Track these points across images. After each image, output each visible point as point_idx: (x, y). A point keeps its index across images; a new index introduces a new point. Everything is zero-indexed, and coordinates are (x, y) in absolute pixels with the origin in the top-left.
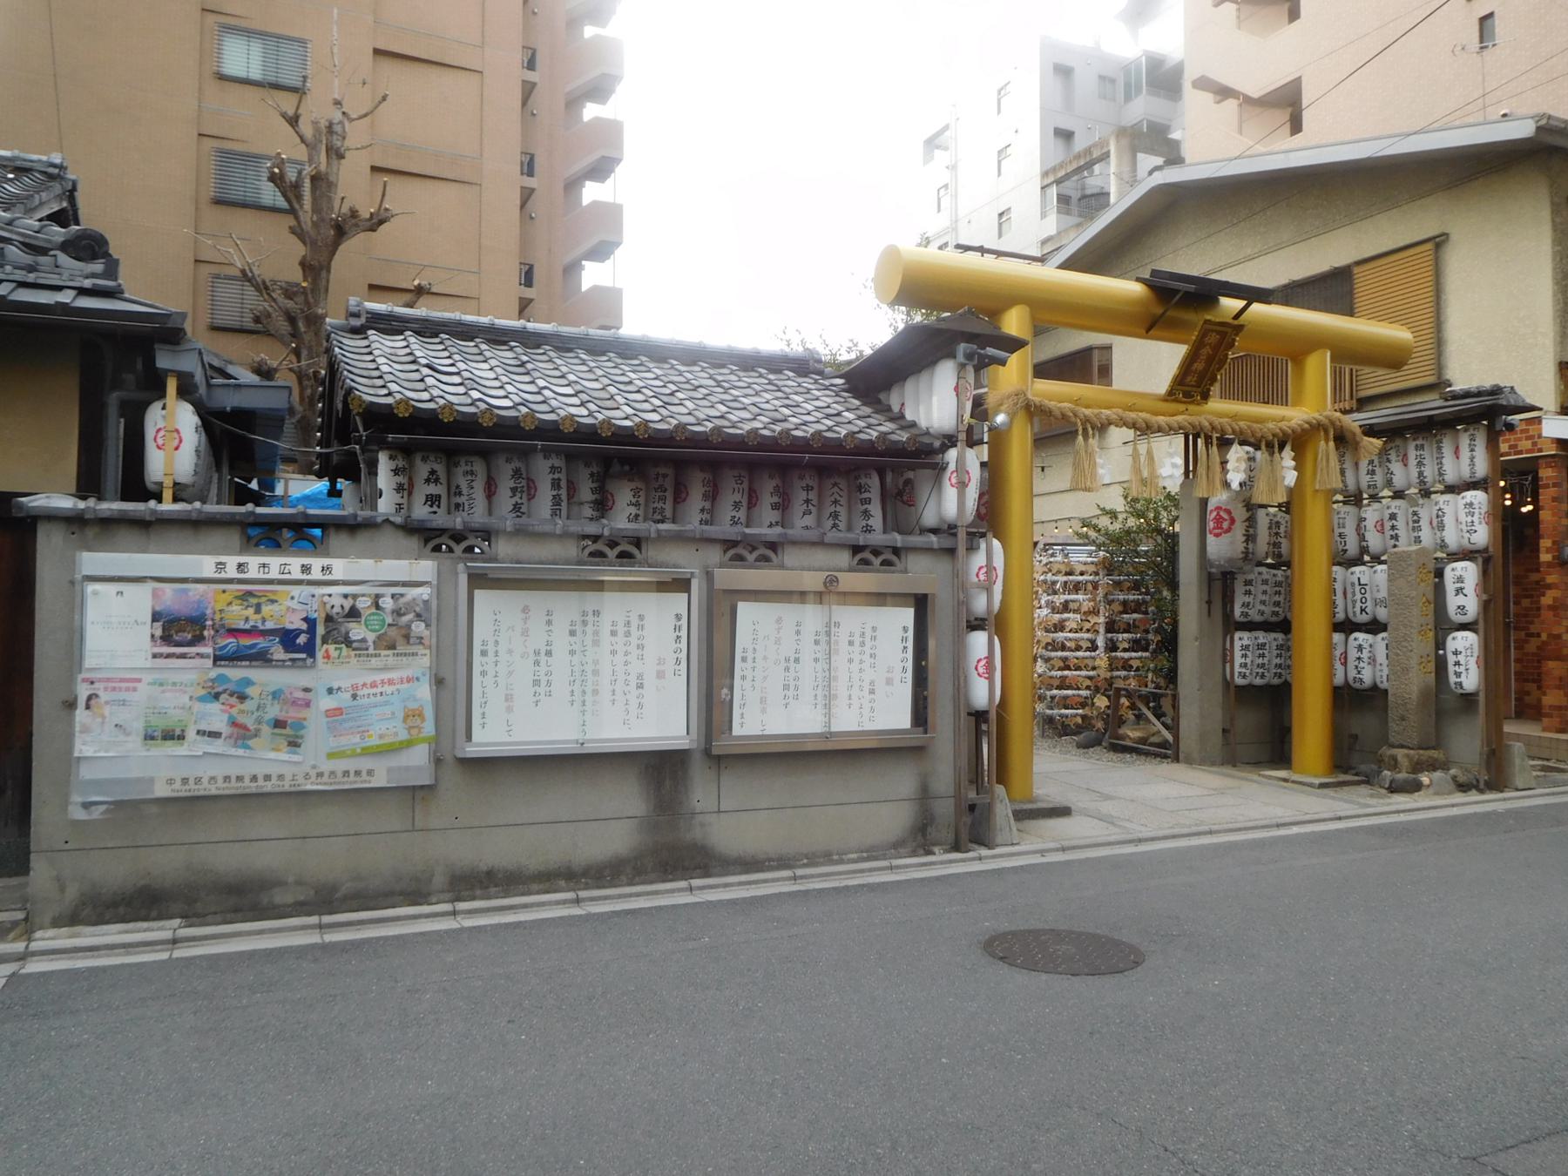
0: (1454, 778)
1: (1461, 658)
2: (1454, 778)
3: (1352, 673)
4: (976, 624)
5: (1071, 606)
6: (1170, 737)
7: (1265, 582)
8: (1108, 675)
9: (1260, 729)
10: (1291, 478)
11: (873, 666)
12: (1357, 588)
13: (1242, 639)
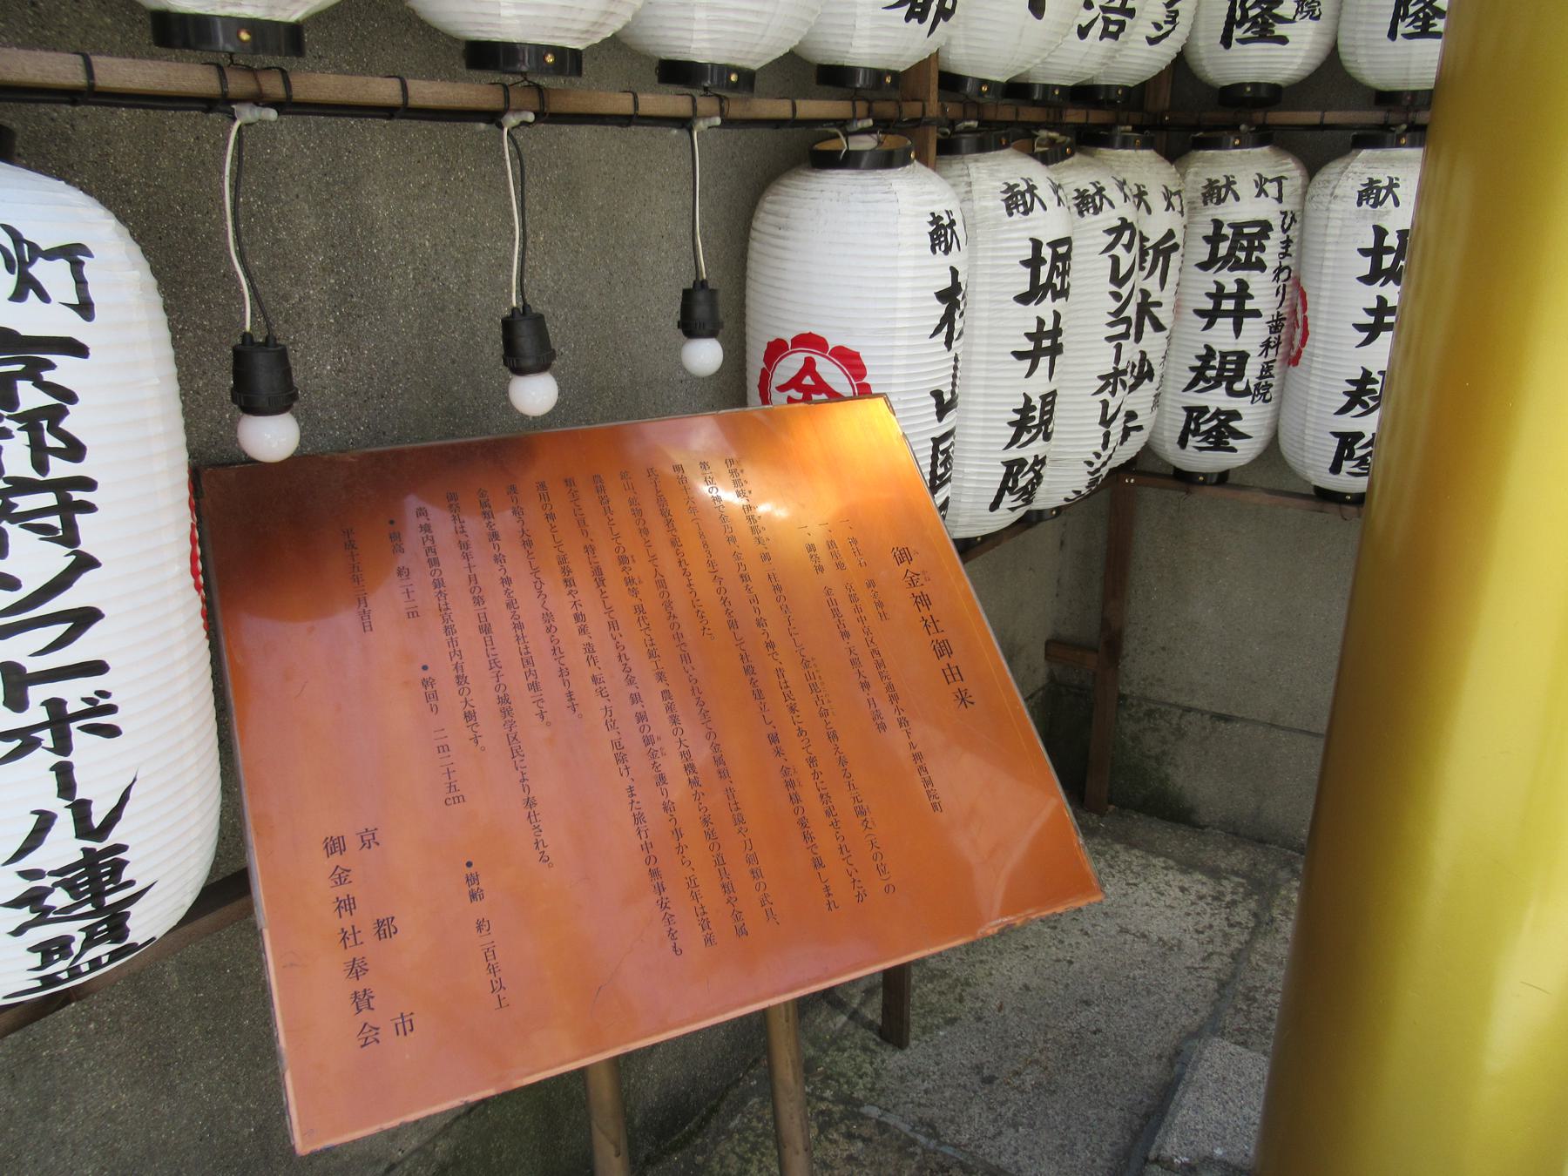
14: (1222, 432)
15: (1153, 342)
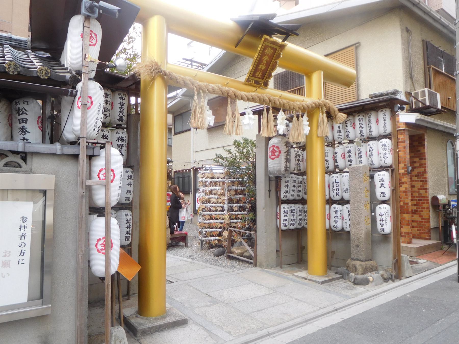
0: (382, 276)
1: (383, 217)
2: (382, 276)
3: (333, 224)
4: (98, 211)
5: (213, 192)
6: (253, 254)
7: (294, 181)
8: (229, 222)
9: (294, 249)
10: (307, 130)
12: (335, 184)
13: (285, 208)
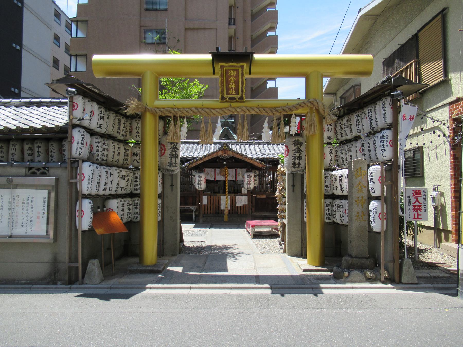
11: (32, 212)
14: (137, 218)
15: (131, 211)
